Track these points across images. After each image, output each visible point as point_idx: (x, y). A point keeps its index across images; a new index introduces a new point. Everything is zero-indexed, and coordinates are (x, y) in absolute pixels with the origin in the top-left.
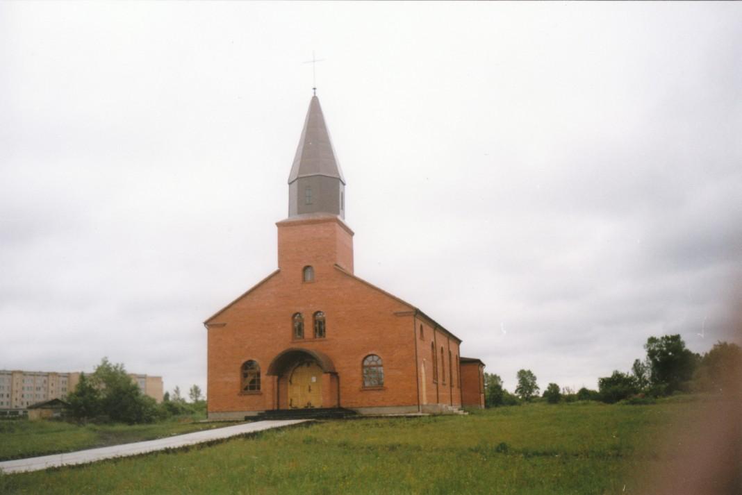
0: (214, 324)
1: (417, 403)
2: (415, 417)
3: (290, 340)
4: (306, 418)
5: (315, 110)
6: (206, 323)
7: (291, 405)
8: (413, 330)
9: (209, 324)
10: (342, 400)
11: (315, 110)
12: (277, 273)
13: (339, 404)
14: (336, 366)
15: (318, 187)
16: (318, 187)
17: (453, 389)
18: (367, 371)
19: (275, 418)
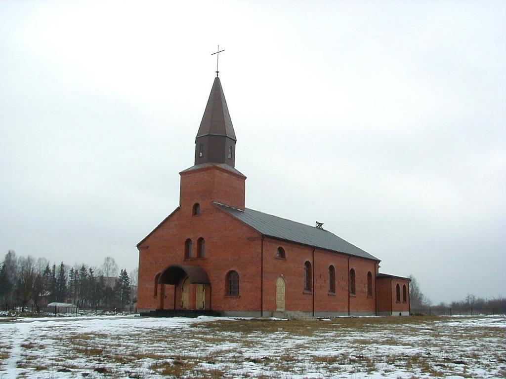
0: (142, 246)
1: (260, 310)
2: (266, 320)
3: (183, 259)
4: (365, 318)
5: (217, 82)
6: (139, 246)
7: (182, 306)
8: (260, 251)
9: (140, 246)
10: (213, 305)
11: (217, 82)
12: (178, 209)
13: (194, 307)
14: (210, 278)
15: (216, 138)
16: (216, 138)
17: (165, 300)
18: (45, 285)
19: (4, 317)
